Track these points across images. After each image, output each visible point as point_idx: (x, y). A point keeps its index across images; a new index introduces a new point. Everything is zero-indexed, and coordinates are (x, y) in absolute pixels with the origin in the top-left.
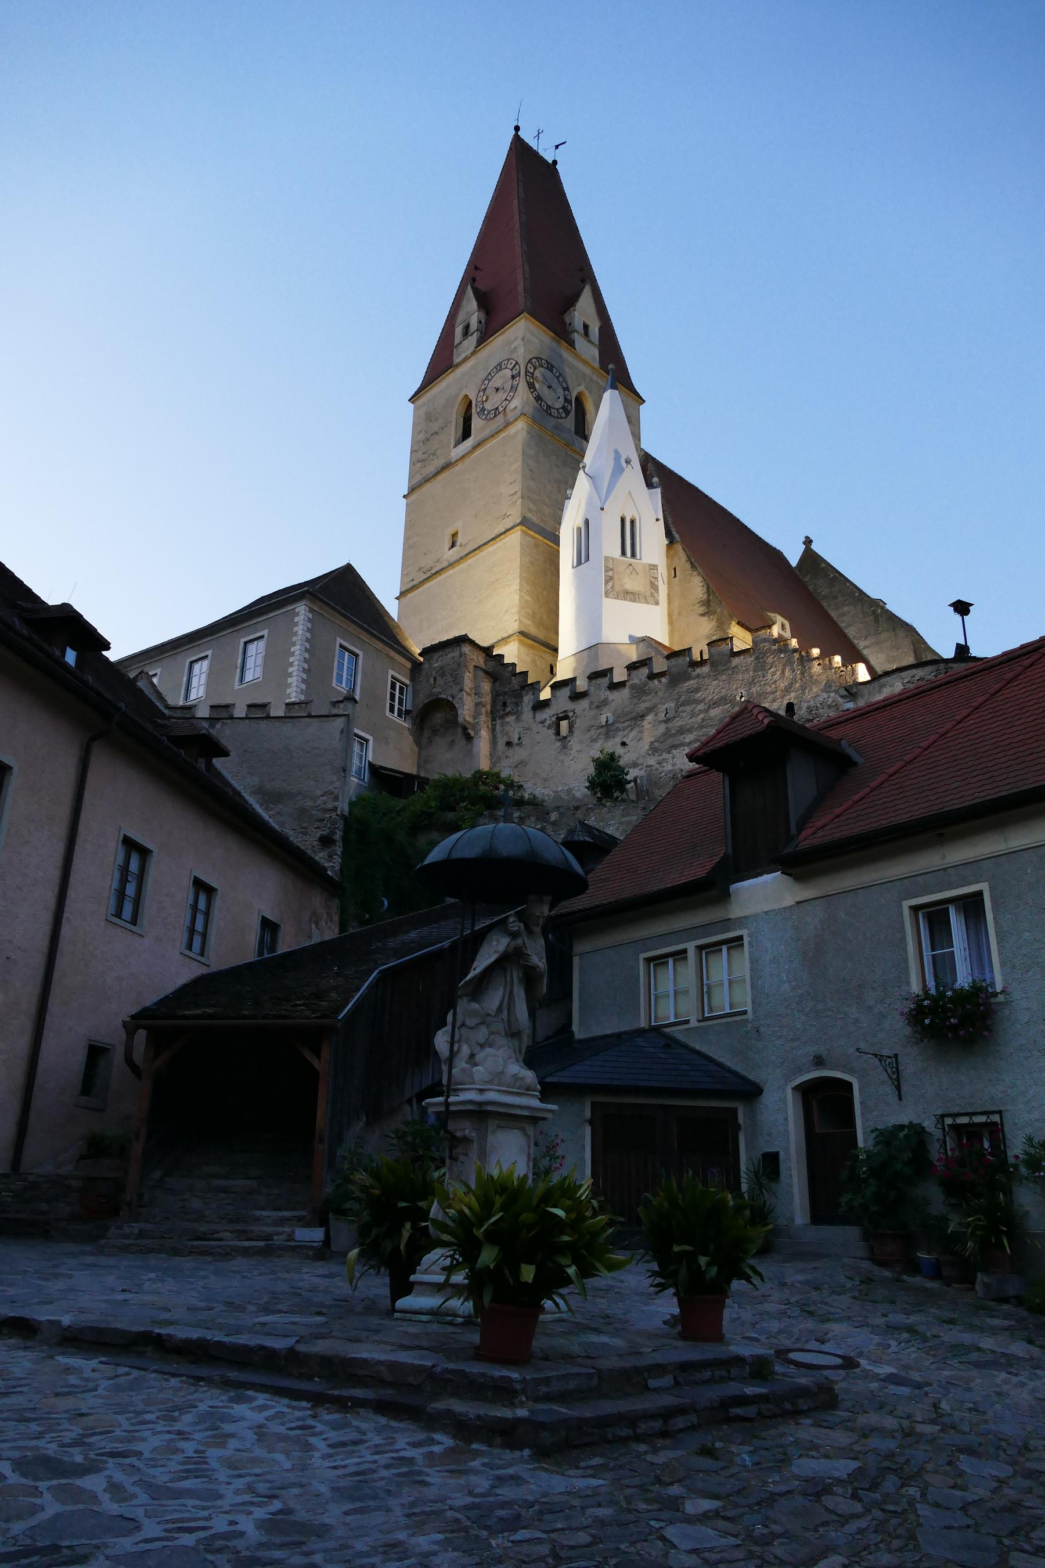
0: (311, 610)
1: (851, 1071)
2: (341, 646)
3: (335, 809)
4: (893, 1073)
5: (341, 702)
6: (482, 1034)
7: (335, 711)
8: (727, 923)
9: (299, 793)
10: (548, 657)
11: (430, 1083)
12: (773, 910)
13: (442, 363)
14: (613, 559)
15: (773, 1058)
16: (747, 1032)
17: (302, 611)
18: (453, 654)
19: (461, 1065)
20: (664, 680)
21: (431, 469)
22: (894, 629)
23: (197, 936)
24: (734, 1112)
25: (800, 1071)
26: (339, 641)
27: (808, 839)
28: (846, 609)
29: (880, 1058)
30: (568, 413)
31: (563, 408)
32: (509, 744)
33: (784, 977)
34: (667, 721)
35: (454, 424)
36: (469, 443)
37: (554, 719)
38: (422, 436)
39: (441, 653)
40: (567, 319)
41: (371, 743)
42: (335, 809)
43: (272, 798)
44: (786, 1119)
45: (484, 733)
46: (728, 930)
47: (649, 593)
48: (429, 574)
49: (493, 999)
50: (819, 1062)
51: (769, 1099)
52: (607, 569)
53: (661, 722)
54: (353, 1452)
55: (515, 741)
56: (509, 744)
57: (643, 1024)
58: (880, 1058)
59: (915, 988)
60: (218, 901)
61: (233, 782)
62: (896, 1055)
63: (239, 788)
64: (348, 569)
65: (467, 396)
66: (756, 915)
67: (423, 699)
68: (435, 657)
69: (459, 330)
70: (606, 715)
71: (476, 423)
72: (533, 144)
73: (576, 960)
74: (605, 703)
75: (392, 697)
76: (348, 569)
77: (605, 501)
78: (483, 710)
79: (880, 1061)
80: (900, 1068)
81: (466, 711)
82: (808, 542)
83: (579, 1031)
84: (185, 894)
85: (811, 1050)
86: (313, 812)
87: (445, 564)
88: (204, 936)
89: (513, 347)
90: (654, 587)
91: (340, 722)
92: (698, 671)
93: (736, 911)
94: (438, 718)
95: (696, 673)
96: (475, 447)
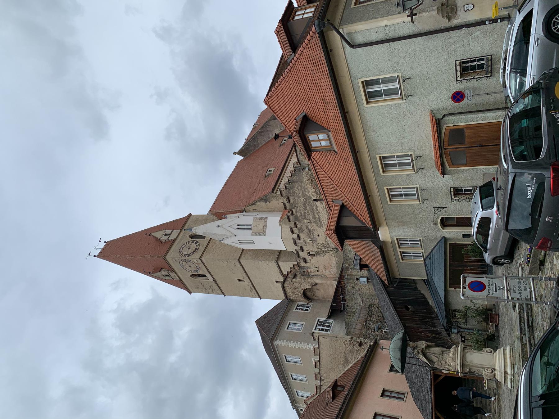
0: (276, 340)
3: (350, 341)
6: (443, 362)
7: (317, 340)
8: (392, 242)
13: (180, 284)
17: (277, 343)
19: (451, 368)
20: (297, 223)
22: (267, 131)
23: (400, 396)
25: (438, 228)
26: (286, 329)
27: (369, 224)
30: (197, 242)
31: (196, 243)
32: (318, 271)
34: (311, 222)
36: (208, 275)
38: (204, 290)
40: (164, 241)
42: (350, 341)
43: (346, 362)
49: (435, 359)
50: (435, 224)
51: (446, 235)
52: (256, 235)
55: (317, 269)
56: (318, 271)
57: (423, 262)
60: (387, 388)
61: (341, 374)
63: (344, 372)
64: (257, 322)
67: (303, 299)
69: (167, 278)
70: (309, 240)
71: (201, 273)
72: (99, 250)
73: (401, 277)
74: (305, 241)
75: (302, 310)
76: (257, 322)
77: (230, 232)
82: (235, 153)
83: (426, 278)
84: (386, 400)
87: (250, 283)
88: (399, 393)
90: (261, 219)
91: (321, 338)
92: (294, 213)
93: (389, 240)
94: (309, 294)
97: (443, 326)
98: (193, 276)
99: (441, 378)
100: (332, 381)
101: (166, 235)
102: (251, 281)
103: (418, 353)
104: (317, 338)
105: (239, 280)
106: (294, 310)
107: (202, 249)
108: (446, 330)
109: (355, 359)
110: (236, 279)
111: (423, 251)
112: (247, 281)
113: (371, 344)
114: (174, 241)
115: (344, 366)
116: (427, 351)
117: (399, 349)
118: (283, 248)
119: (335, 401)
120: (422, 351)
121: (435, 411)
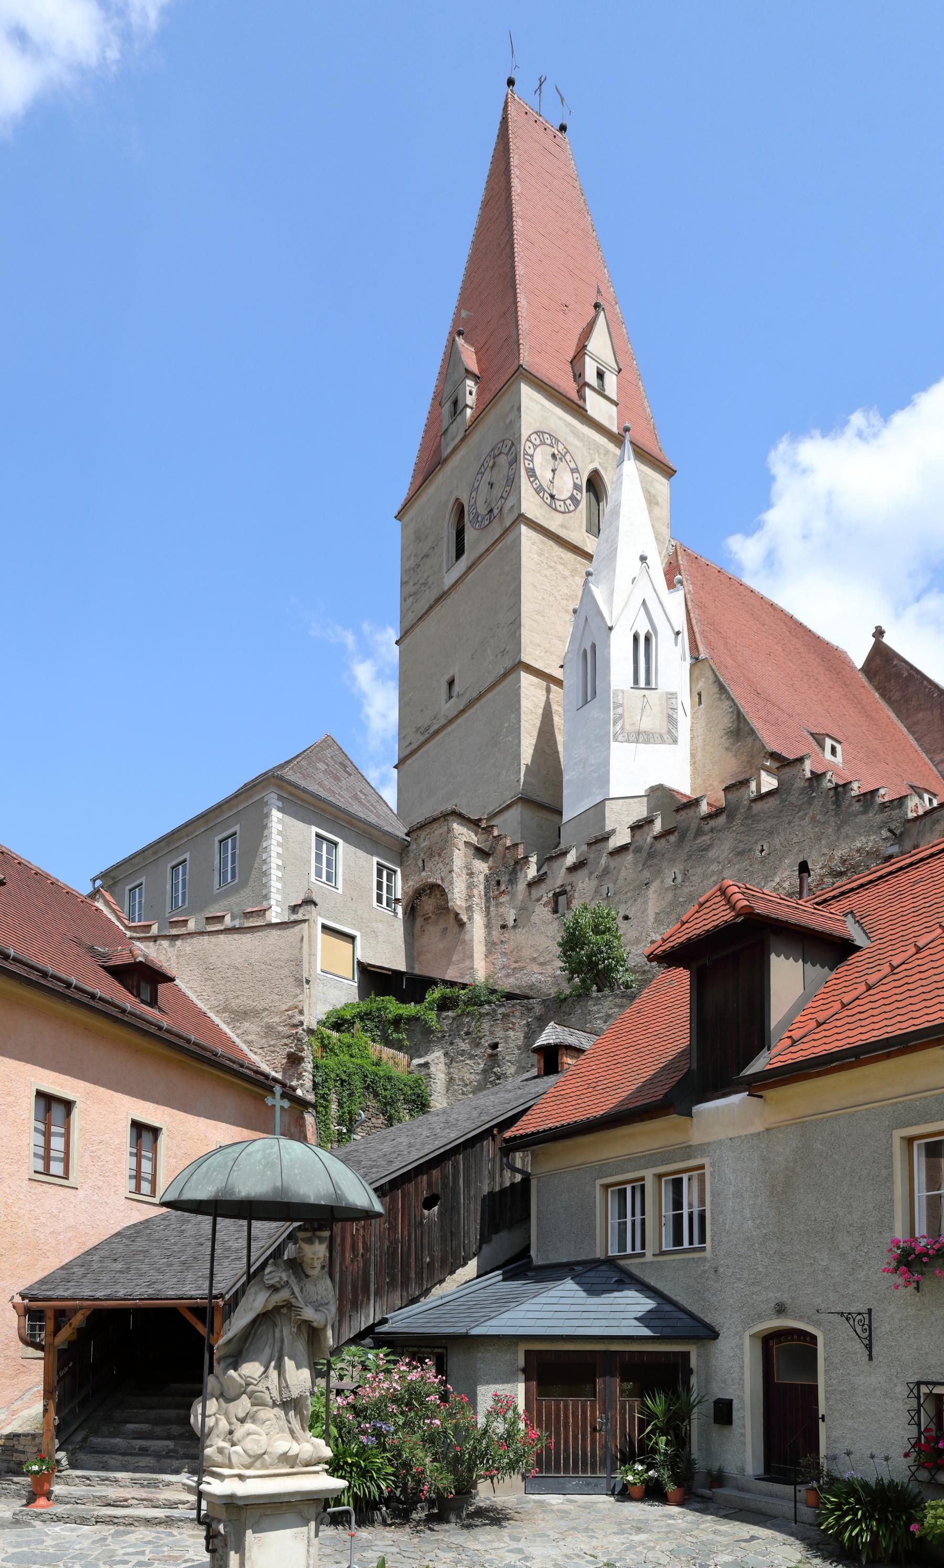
1: (818, 1324)
2: (318, 835)
4: (864, 1331)
5: (300, 905)
7: (294, 917)
9: (265, 1009)
10: (555, 818)
11: (371, 1322)
12: (740, 1137)
14: (623, 692)
15: (731, 1301)
16: (705, 1272)
18: (441, 831)
21: (423, 605)
24: (686, 1355)
25: (760, 1317)
28: (920, 715)
29: (848, 1316)
31: (572, 498)
32: (504, 927)
33: (747, 1212)
35: (445, 540)
37: (551, 895)
38: (412, 563)
39: (428, 830)
41: (358, 941)
42: (302, 1023)
43: (239, 1016)
44: (742, 1368)
45: (479, 919)
46: (689, 1157)
47: (664, 730)
48: (427, 735)
50: (781, 1309)
51: (724, 1347)
53: (667, 889)
54: (532, 1422)
56: (504, 927)
57: (599, 1254)
58: (848, 1316)
59: (900, 1233)
62: (870, 1310)
65: (457, 499)
66: (720, 1142)
68: (422, 836)
71: (470, 534)
75: (379, 885)
78: (475, 892)
79: (848, 1319)
80: (874, 1326)
81: (458, 896)
82: (879, 633)
85: (774, 1296)
86: (280, 1029)
87: (443, 721)
89: (508, 421)
90: (672, 720)
95: (709, 825)
96: (470, 568)
97: (384, 1321)
98: (460, 511)
99: (202, 1329)
100: (171, 970)
101: (600, 375)
102: (451, 721)
103: (275, 1289)
104: (299, 916)
105: (451, 683)
106: (376, 859)
107: (554, 523)
108: (370, 1330)
109: (249, 1043)
110: (454, 670)
111: (649, 1257)
112: (449, 708)
113: (299, 1092)
114: (578, 410)
115: (224, 1009)
116: (287, 1331)
117: (283, 1190)
118: (566, 817)
119: (103, 973)
120: (288, 1305)
121: (87, 1308)
